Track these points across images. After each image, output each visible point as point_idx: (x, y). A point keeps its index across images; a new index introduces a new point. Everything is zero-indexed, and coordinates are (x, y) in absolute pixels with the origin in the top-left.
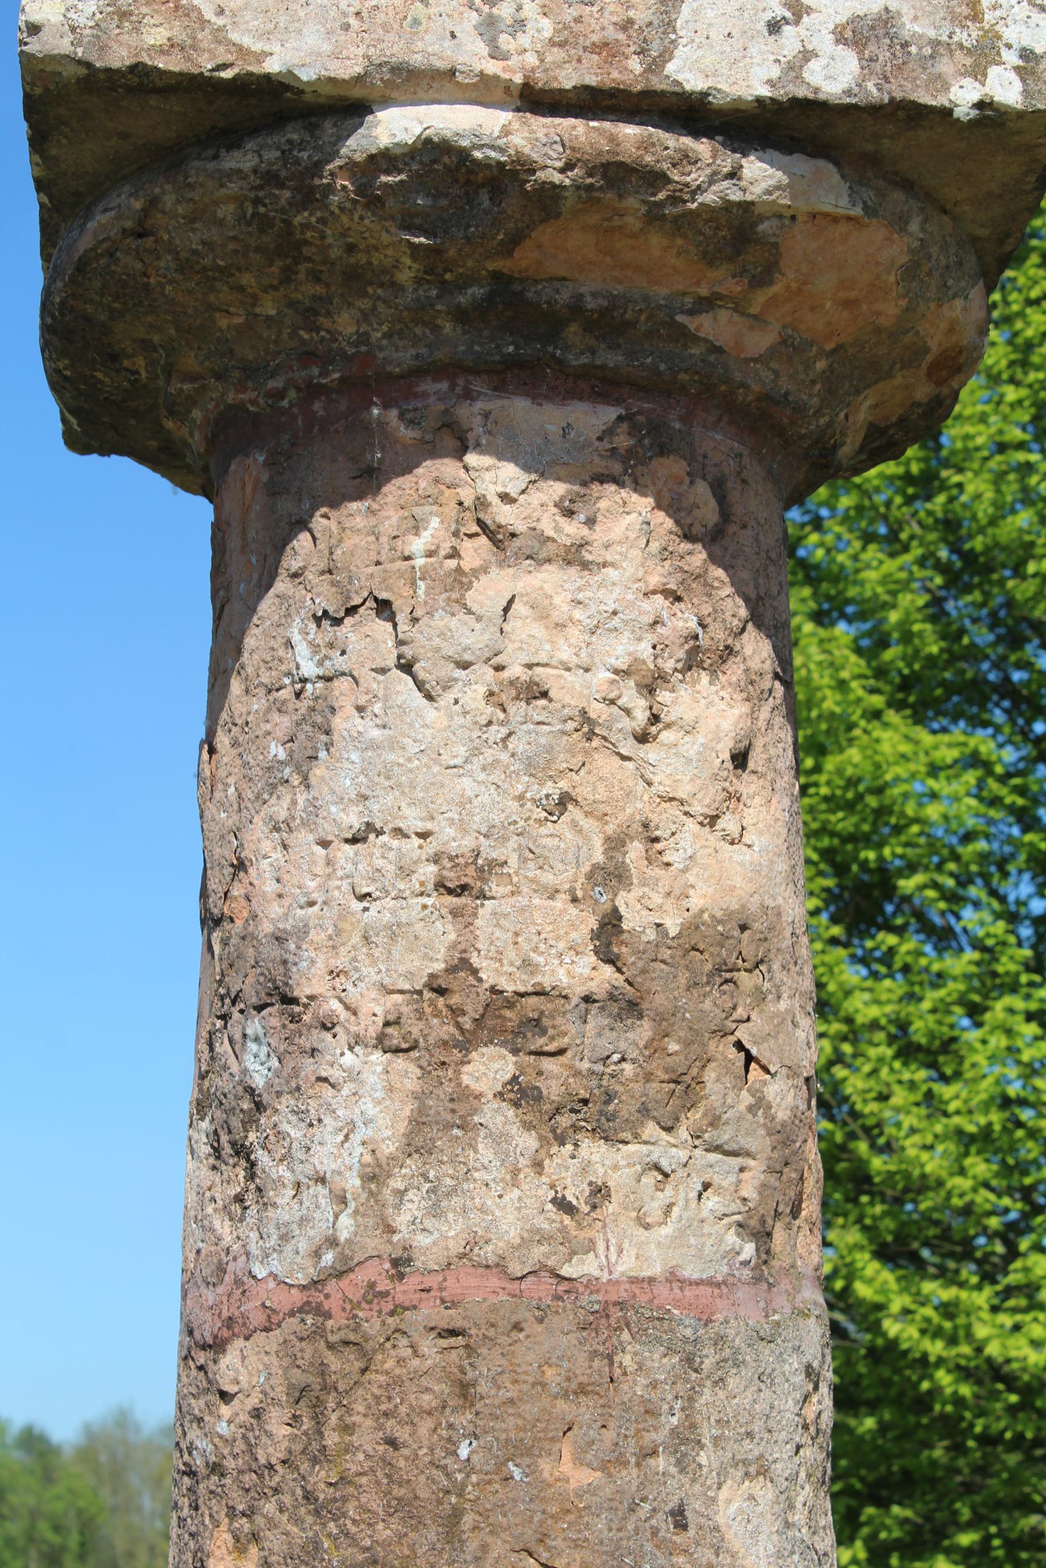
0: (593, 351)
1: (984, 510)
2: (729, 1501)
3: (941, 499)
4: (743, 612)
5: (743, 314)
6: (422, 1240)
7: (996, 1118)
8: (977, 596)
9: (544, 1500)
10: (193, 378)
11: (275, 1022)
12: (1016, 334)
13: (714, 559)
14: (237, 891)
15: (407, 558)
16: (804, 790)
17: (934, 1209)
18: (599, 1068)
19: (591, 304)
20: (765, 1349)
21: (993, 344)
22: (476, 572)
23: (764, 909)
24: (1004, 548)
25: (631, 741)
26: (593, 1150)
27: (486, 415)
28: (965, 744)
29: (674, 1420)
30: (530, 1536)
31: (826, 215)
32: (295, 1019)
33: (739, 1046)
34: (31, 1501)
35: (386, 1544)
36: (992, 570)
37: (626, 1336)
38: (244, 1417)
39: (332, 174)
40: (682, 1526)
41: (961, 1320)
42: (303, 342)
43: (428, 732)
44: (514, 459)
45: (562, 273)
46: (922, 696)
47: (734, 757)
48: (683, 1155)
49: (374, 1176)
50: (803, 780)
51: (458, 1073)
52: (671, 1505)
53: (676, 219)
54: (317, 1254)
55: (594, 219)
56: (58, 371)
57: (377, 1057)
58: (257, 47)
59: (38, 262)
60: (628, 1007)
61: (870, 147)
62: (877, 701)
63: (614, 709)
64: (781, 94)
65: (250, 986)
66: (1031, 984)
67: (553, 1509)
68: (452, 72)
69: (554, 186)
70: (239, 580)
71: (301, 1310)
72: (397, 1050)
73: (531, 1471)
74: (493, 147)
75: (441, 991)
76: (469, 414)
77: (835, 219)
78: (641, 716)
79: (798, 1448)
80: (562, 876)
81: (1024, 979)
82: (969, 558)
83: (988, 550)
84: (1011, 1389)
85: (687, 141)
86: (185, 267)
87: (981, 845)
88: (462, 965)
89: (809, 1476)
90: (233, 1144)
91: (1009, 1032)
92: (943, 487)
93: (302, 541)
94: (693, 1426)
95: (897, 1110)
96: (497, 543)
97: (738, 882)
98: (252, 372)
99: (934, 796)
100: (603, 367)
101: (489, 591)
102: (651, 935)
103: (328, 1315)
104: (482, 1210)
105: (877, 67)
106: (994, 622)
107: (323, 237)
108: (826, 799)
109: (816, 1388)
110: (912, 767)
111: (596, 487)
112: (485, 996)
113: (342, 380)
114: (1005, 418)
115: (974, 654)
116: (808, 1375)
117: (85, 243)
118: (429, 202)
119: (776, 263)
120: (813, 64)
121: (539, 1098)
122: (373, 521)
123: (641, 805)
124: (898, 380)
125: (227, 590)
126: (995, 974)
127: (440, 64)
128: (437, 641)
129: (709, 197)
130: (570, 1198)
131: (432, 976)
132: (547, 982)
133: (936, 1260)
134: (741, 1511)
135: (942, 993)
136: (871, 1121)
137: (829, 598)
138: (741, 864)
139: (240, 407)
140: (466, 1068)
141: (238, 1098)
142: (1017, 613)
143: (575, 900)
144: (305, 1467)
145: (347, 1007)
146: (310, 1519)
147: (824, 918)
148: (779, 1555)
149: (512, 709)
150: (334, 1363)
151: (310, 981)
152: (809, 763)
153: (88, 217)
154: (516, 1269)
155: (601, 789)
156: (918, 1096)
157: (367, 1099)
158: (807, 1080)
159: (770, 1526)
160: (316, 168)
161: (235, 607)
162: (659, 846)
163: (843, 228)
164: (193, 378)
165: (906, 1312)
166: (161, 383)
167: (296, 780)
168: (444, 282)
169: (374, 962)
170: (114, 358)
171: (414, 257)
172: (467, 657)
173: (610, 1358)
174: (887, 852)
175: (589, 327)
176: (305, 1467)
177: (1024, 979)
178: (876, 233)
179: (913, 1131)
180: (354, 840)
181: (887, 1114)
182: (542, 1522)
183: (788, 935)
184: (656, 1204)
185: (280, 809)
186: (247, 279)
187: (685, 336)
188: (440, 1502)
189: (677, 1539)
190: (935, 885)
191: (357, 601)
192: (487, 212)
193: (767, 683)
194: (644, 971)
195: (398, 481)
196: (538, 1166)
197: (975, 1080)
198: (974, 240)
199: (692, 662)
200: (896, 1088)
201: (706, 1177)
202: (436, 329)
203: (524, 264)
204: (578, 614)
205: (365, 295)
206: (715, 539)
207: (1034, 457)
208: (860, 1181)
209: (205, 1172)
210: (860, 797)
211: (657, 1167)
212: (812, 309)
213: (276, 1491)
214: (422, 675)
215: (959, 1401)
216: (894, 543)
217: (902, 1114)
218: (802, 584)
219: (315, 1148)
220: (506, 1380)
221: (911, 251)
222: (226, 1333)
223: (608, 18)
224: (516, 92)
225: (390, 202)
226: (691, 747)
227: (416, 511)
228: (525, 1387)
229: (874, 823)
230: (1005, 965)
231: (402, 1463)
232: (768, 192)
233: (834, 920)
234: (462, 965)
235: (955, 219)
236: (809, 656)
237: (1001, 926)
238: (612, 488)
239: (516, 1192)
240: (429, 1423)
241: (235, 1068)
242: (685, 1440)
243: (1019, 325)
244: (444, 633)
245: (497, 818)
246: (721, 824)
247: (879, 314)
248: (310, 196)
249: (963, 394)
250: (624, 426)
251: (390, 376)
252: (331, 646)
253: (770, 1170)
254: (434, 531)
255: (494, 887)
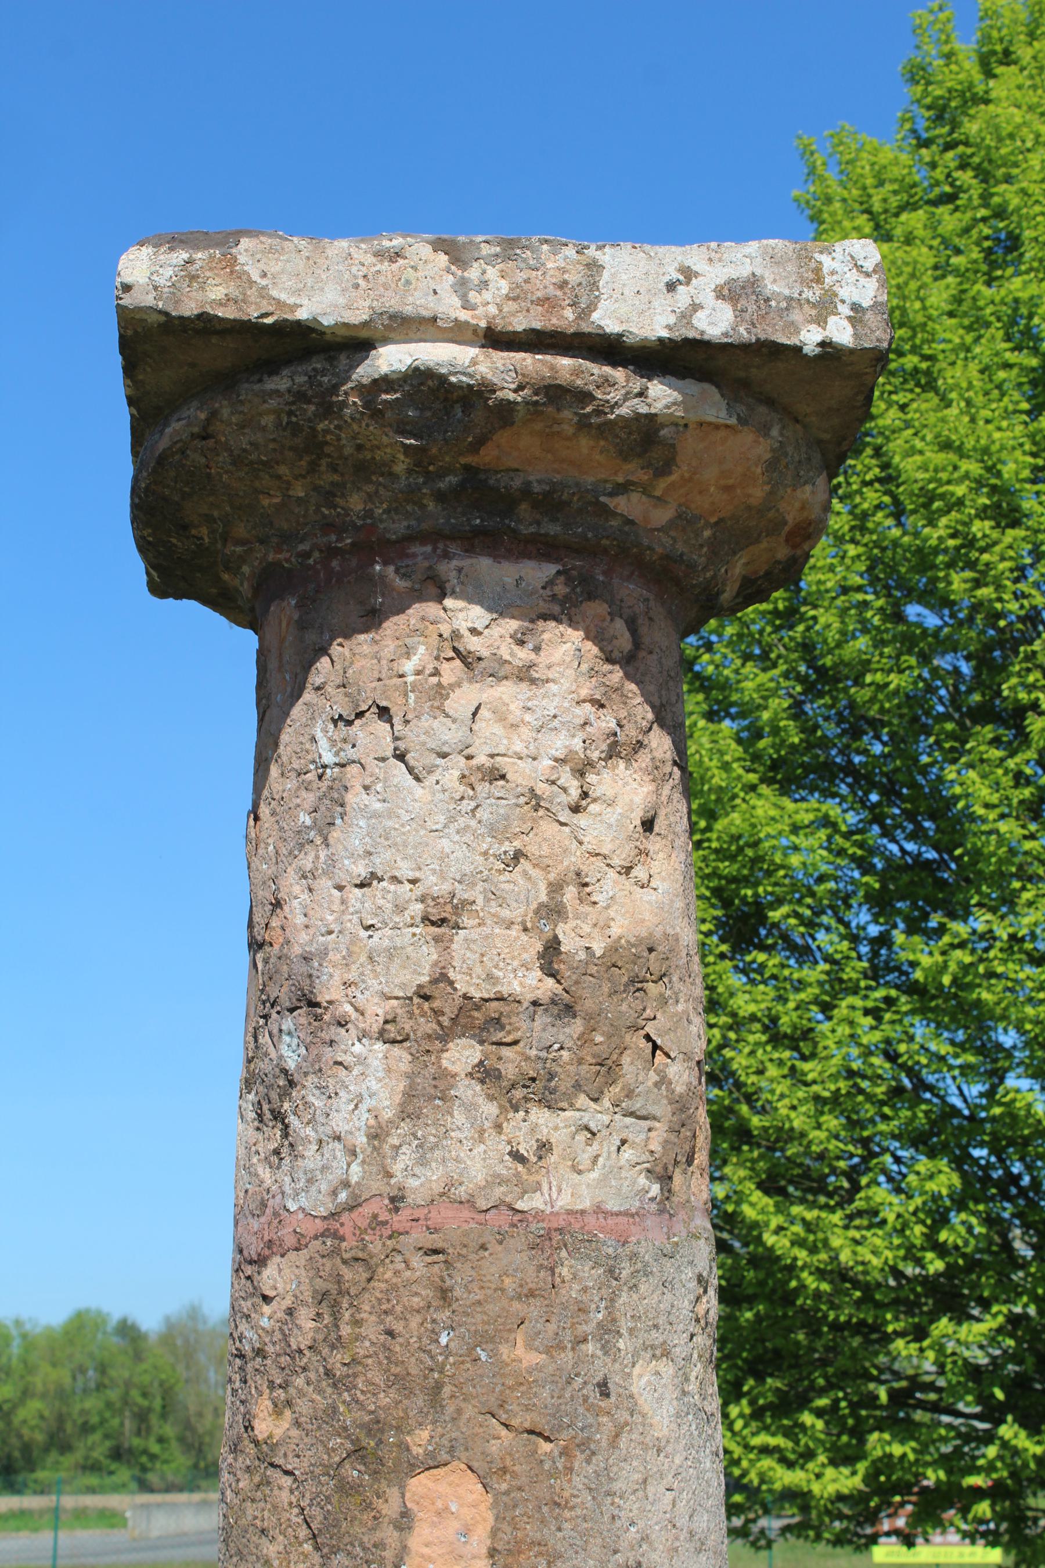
0: (538, 523)
1: (832, 636)
2: (640, 1376)
3: (801, 628)
4: (650, 716)
5: (650, 496)
6: (413, 1183)
7: (843, 1085)
8: (827, 700)
9: (504, 1375)
10: (242, 542)
11: (303, 1020)
12: (856, 506)
13: (628, 676)
14: (275, 923)
15: (401, 676)
16: (698, 845)
17: (797, 1155)
18: (543, 1054)
19: (537, 488)
20: (668, 1263)
21: (838, 513)
22: (452, 687)
23: (666, 935)
24: (847, 665)
25: (567, 811)
26: (540, 1116)
27: (460, 570)
28: (818, 810)
29: (600, 1316)
30: (493, 1402)
31: (710, 424)
32: (318, 1018)
33: (648, 1038)
34: (126, 1374)
35: (386, 1408)
36: (839, 681)
37: (564, 1253)
38: (280, 1315)
39: (346, 393)
40: (606, 1394)
41: (820, 1235)
42: (324, 516)
43: (417, 805)
44: (480, 603)
45: (516, 466)
46: (786, 775)
47: (643, 823)
48: (606, 1119)
49: (376, 1136)
50: (697, 837)
51: (439, 1058)
52: (598, 1378)
53: (599, 426)
54: (334, 1193)
55: (538, 426)
56: (143, 538)
57: (379, 1046)
58: (291, 301)
59: (129, 457)
61: (742, 374)
62: (753, 778)
63: (555, 788)
64: (676, 335)
65: (284, 993)
66: (868, 988)
67: (510, 1382)
68: (435, 319)
69: (509, 402)
70: (277, 690)
71: (322, 1235)
72: (394, 1042)
73: (494, 1354)
74: (464, 374)
75: (426, 998)
76: (448, 569)
77: (717, 427)
78: (575, 793)
79: (692, 1336)
80: (516, 912)
81: (863, 984)
82: (822, 672)
83: (835, 665)
84: (855, 1288)
85: (607, 370)
86: (237, 461)
87: (831, 885)
88: (442, 978)
89: (700, 1356)
90: (272, 1111)
91: (851, 1023)
92: (802, 619)
93: (324, 662)
94: (614, 1320)
95: (772, 1080)
96: (468, 665)
97: (647, 916)
98: (287, 538)
99: (796, 848)
100: (546, 535)
101: (461, 702)
102: (582, 955)
103: (342, 1239)
104: (457, 1160)
105: (747, 316)
106: (841, 719)
107: (339, 439)
108: (716, 851)
109: (705, 1292)
110: (779, 826)
111: (541, 623)
112: (459, 1001)
113: (353, 544)
114: (848, 568)
115: (825, 743)
116: (699, 1282)
117: (163, 444)
118: (418, 413)
119: (674, 459)
120: (700, 314)
121: (499, 1077)
122: (376, 648)
123: (575, 859)
124: (764, 545)
125: (268, 699)
126: (841, 981)
127: (426, 313)
128: (423, 737)
129: (624, 411)
130: (522, 1151)
131: (419, 986)
132: (505, 991)
133: (798, 1193)
134: (649, 1382)
135: (802, 996)
136: (750, 1090)
137: (718, 702)
138: (649, 902)
139: (278, 564)
140: (445, 1055)
141: (275, 1077)
142: (857, 713)
143: (525, 930)
144: (326, 1351)
145: (357, 1010)
146: (329, 1390)
147: (715, 939)
148: (678, 1415)
149: (479, 788)
150: (347, 1274)
151: (329, 989)
152: (703, 824)
153: (166, 425)
154: (483, 1204)
155: (545, 847)
156: (786, 1071)
157: (370, 1079)
158: (699, 1063)
159: (670, 1394)
160: (334, 389)
161: (274, 711)
162: (588, 889)
163: (722, 433)
164: (242, 542)
165: (780, 1229)
166: (219, 546)
167: (318, 841)
168: (428, 472)
169: (376, 976)
170: (185, 527)
171: (406, 454)
172: (445, 749)
173: (552, 1270)
174: (761, 890)
175: (536, 505)
176: (326, 1351)
177: (863, 984)
178: (747, 437)
179: (782, 1096)
180: (361, 885)
181: (764, 1084)
182: (502, 1392)
183: (684, 954)
184: (586, 1156)
185: (307, 862)
186: (283, 470)
187: (607, 512)
188: (426, 1377)
189: (602, 1404)
190: (796, 915)
191: (364, 707)
192: (459, 421)
193: (668, 768)
194: (577, 983)
195: (395, 619)
196: (498, 1127)
197: (827, 1058)
198: (820, 442)
199: (613, 752)
200: (768, 1065)
201: (624, 1136)
202: (423, 507)
203: (487, 459)
204: (528, 717)
205: (371, 482)
206: (629, 662)
207: (870, 597)
208: (744, 1135)
209: (251, 1131)
210: (740, 850)
211: (587, 1128)
212: (700, 492)
213: (304, 1369)
214: (412, 763)
215: (818, 1295)
216: (765, 661)
217: (774, 1083)
218: (697, 691)
219: (333, 1114)
220: (475, 1286)
221: (773, 450)
222: (267, 1252)
223: (549, 280)
224: (481, 334)
225: (389, 414)
226: (612, 815)
227: (408, 641)
228: (489, 1292)
229: (751, 869)
230: (849, 974)
231: (398, 1349)
232: (667, 407)
233: (723, 940)
234: (442, 978)
235: (805, 426)
236: (700, 745)
237: (845, 944)
238: (553, 624)
239: (482, 1147)
240: (418, 1318)
241: (273, 1054)
242: (608, 1330)
243: (858, 500)
244: (428, 731)
245: (468, 869)
246: (634, 873)
247: (749, 496)
248: (329, 409)
249: (816, 551)
250: (562, 578)
251: (388, 541)
252: (345, 741)
253: (671, 1130)
254: (421, 656)
255: (466, 920)
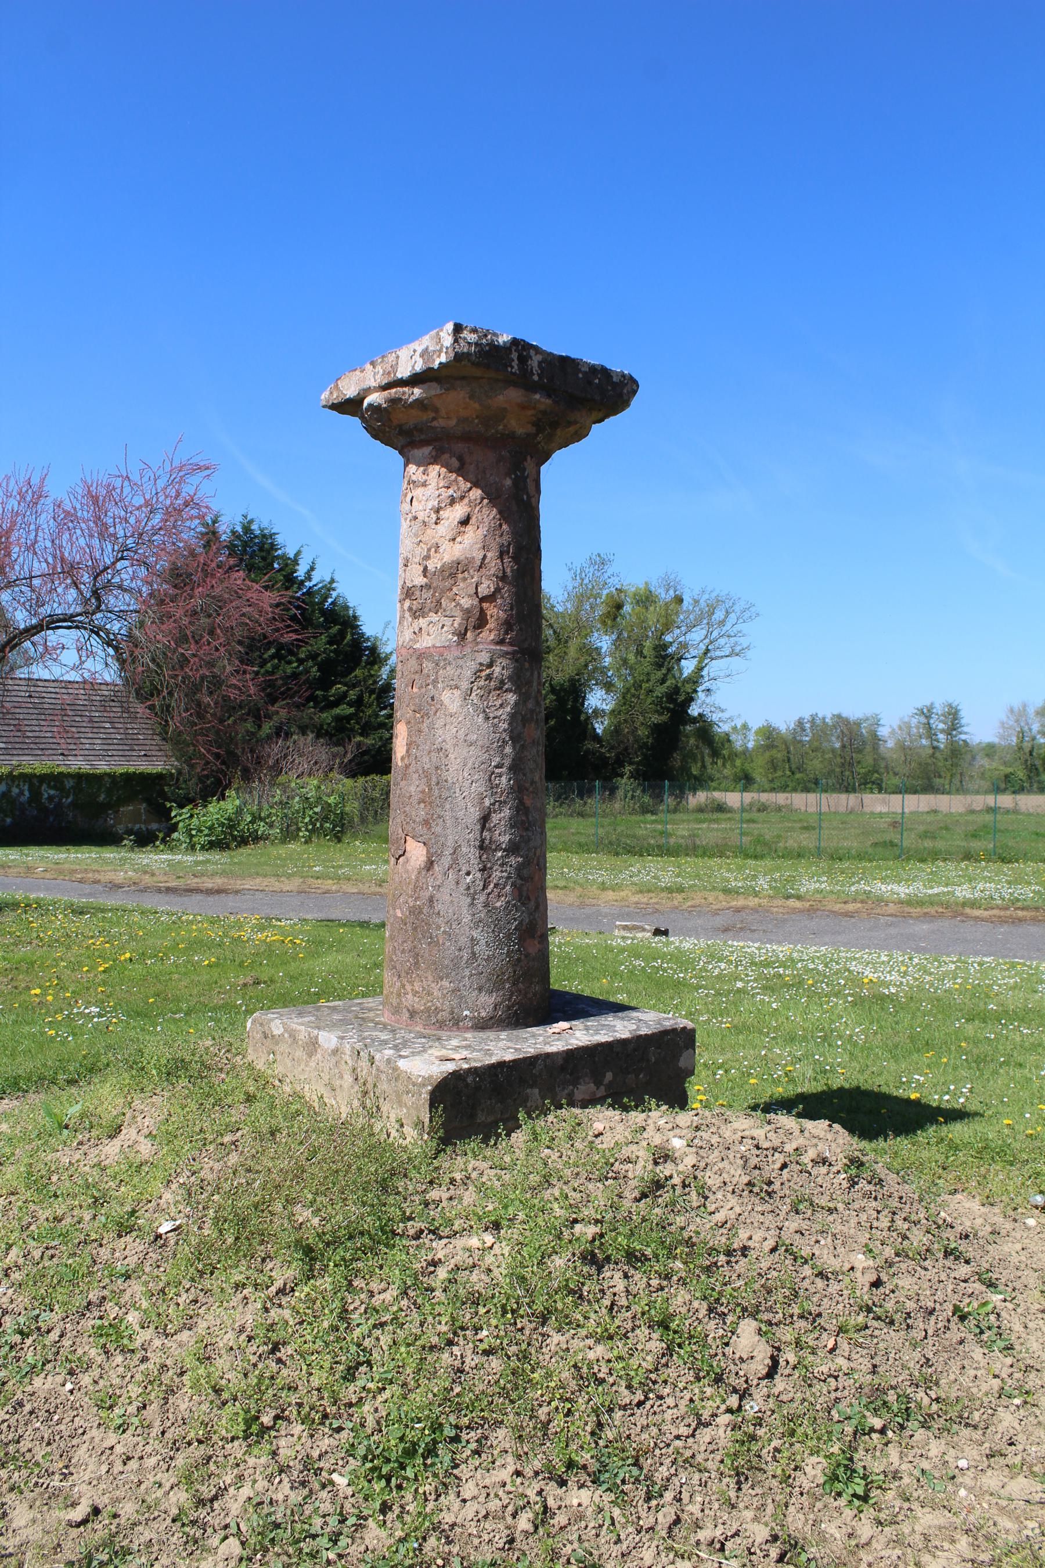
60: (428, 587)
242: (435, 682)
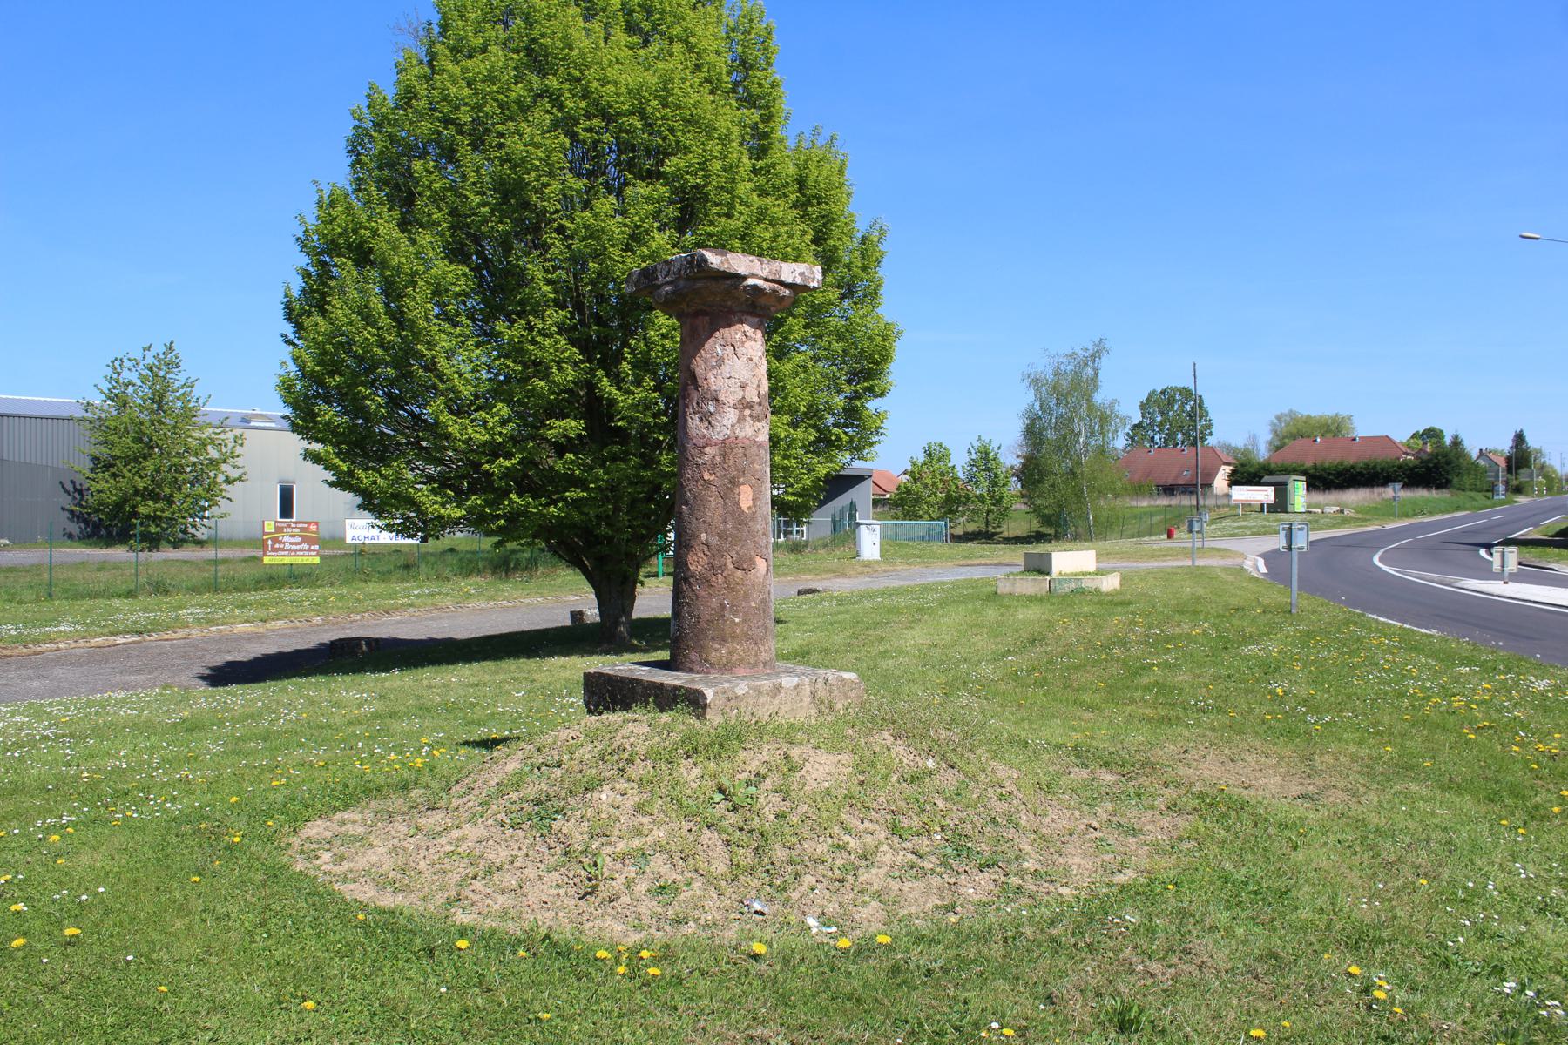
151: (722, 397)
